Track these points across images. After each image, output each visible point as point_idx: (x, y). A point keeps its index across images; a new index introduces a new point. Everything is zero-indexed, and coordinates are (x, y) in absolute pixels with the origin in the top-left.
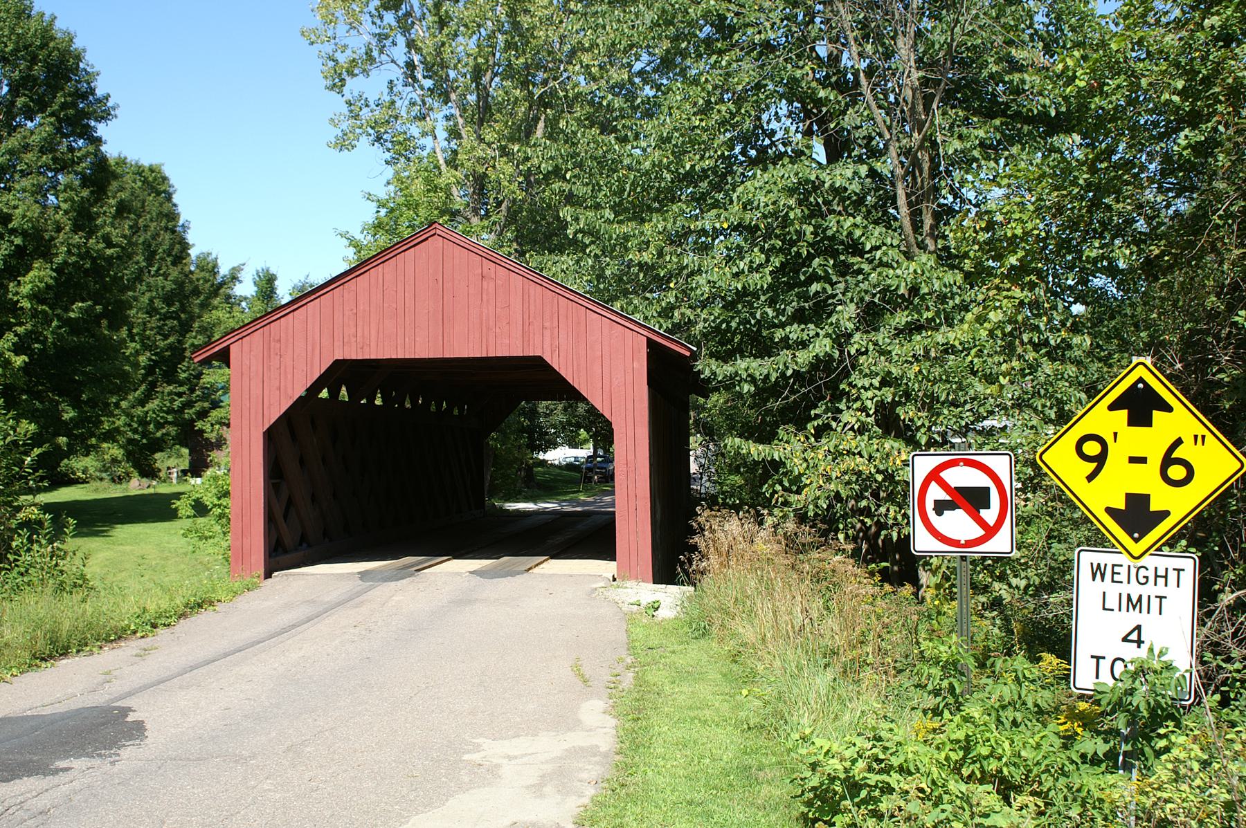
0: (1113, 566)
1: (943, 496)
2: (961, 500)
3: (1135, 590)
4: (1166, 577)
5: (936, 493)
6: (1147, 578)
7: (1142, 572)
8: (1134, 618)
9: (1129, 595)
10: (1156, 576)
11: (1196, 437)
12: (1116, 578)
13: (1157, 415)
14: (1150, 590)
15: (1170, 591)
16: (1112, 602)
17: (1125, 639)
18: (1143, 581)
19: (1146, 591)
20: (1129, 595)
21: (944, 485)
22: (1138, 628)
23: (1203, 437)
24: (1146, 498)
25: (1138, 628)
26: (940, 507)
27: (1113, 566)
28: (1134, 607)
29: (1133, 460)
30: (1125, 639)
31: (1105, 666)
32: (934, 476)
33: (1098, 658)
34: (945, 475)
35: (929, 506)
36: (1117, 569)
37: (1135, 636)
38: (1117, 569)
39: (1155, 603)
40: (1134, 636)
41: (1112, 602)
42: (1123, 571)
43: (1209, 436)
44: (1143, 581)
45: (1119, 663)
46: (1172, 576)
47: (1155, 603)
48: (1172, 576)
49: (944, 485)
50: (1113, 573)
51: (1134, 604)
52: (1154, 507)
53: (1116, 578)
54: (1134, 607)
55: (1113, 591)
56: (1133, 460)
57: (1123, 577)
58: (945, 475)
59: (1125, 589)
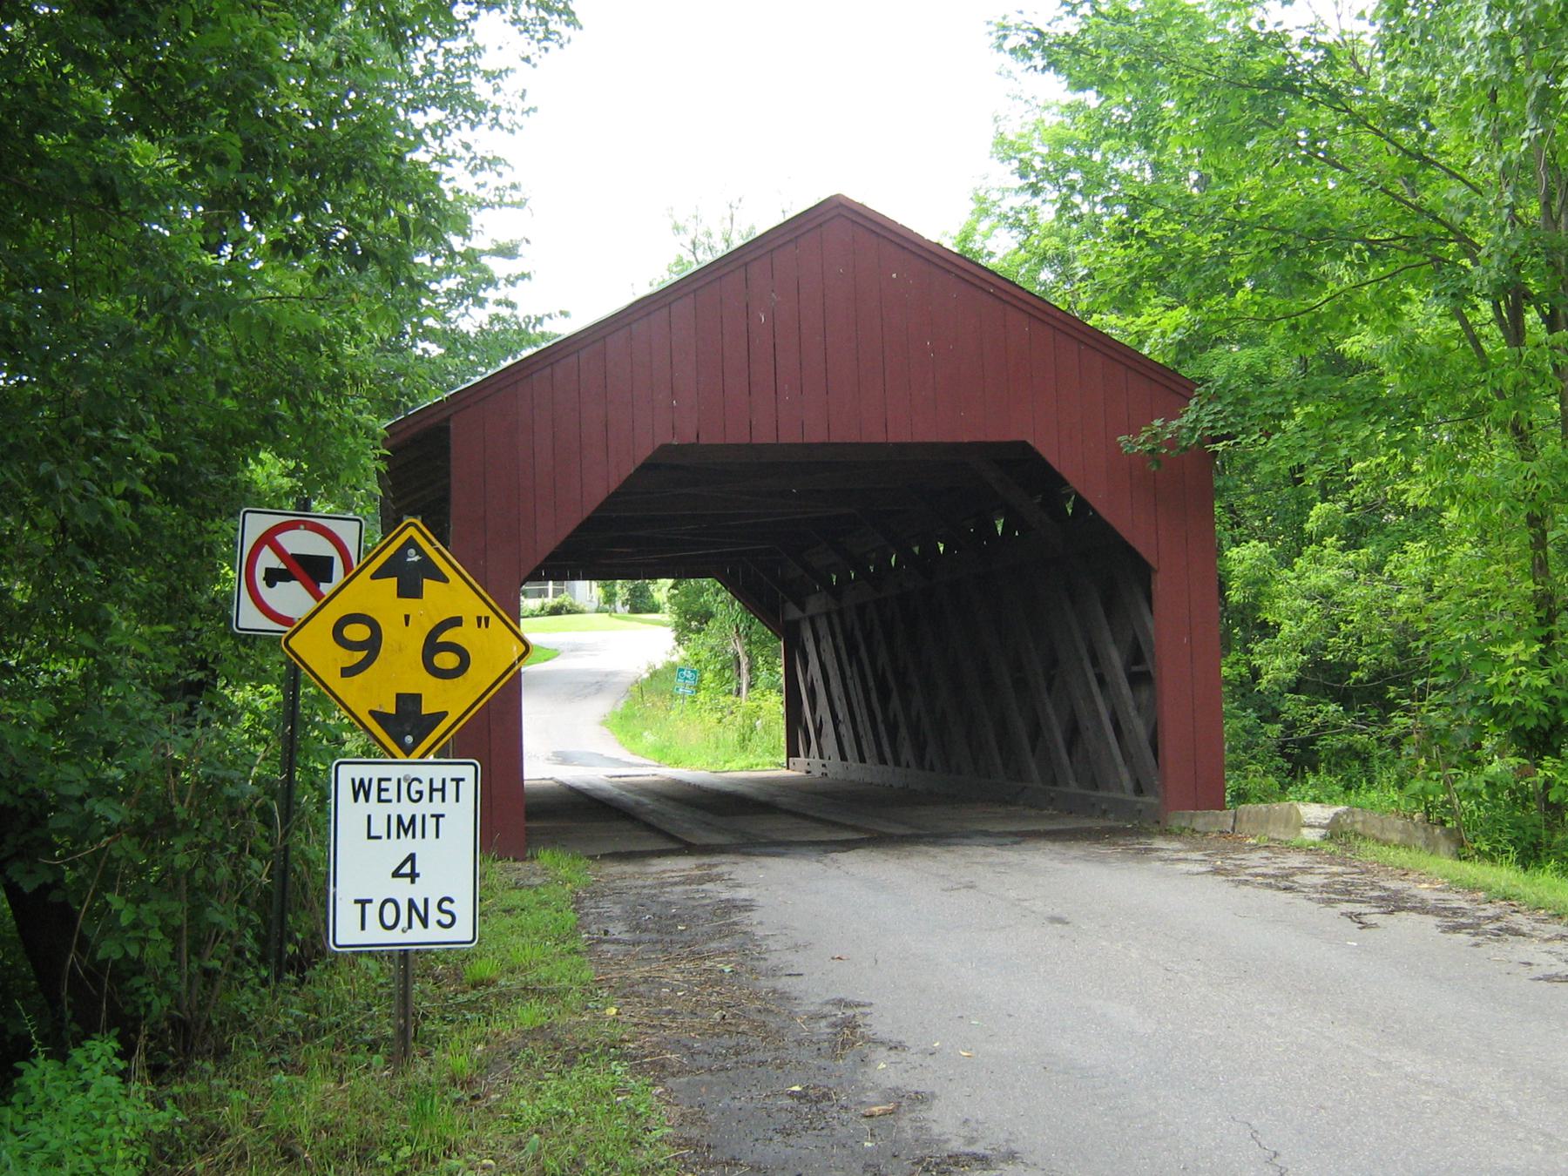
0: (380, 780)
1: (276, 563)
2: (297, 570)
3: (406, 809)
4: (443, 790)
5: (268, 560)
6: (420, 793)
7: (415, 786)
8: (406, 845)
9: (399, 817)
10: (432, 790)
11: (479, 619)
12: (384, 796)
13: (391, 709)
14: (424, 808)
15: (448, 807)
16: (379, 828)
17: (396, 874)
18: (416, 797)
19: (424, 808)
20: (399, 817)
21: (279, 551)
22: (412, 858)
23: (487, 619)
24: (417, 698)
25: (412, 858)
26: (272, 577)
27: (380, 780)
28: (406, 833)
29: (407, 617)
30: (396, 874)
31: (373, 911)
32: (268, 538)
33: (363, 903)
34: (281, 538)
35: (259, 574)
36: (384, 785)
37: (408, 870)
38: (384, 785)
39: (431, 823)
40: (407, 869)
41: (379, 828)
42: (392, 786)
43: (493, 619)
44: (416, 797)
45: (389, 922)
46: (450, 787)
47: (431, 823)
48: (450, 787)
49: (279, 551)
50: (380, 790)
51: (406, 827)
52: (426, 709)
53: (384, 796)
54: (406, 833)
55: (379, 812)
56: (407, 617)
57: (392, 794)
58: (281, 538)
59: (394, 809)
